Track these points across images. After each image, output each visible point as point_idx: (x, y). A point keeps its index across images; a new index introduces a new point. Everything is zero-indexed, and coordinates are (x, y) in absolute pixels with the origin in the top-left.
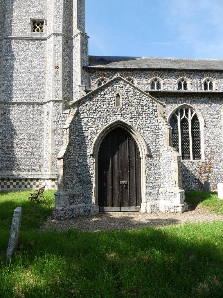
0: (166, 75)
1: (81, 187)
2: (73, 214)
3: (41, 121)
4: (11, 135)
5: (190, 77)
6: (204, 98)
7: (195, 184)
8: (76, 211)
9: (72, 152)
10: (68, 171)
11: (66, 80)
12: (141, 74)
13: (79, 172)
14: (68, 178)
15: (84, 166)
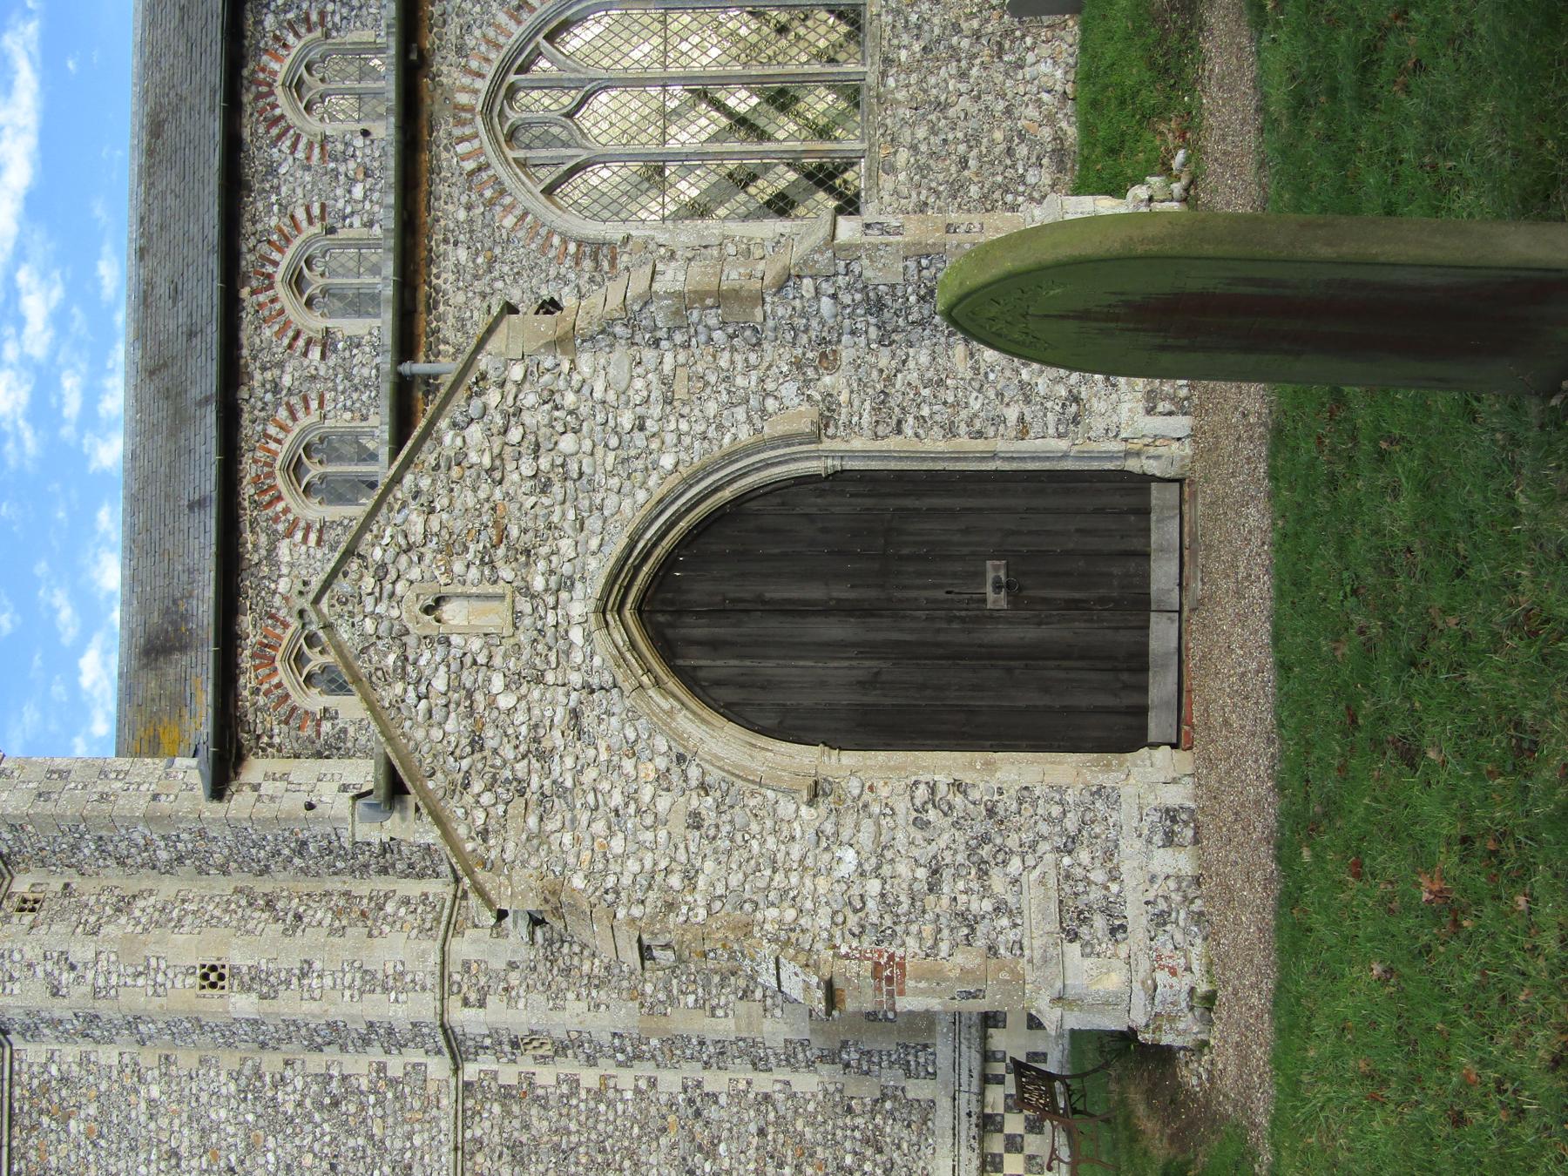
0: (269, 212)
1: (1015, 864)
2: (1182, 923)
3: (583, 1095)
5: (276, 38)
7: (1030, 57)
8: (1166, 898)
9: (790, 914)
10: (911, 942)
12: (259, 392)
13: (922, 873)
15: (884, 839)
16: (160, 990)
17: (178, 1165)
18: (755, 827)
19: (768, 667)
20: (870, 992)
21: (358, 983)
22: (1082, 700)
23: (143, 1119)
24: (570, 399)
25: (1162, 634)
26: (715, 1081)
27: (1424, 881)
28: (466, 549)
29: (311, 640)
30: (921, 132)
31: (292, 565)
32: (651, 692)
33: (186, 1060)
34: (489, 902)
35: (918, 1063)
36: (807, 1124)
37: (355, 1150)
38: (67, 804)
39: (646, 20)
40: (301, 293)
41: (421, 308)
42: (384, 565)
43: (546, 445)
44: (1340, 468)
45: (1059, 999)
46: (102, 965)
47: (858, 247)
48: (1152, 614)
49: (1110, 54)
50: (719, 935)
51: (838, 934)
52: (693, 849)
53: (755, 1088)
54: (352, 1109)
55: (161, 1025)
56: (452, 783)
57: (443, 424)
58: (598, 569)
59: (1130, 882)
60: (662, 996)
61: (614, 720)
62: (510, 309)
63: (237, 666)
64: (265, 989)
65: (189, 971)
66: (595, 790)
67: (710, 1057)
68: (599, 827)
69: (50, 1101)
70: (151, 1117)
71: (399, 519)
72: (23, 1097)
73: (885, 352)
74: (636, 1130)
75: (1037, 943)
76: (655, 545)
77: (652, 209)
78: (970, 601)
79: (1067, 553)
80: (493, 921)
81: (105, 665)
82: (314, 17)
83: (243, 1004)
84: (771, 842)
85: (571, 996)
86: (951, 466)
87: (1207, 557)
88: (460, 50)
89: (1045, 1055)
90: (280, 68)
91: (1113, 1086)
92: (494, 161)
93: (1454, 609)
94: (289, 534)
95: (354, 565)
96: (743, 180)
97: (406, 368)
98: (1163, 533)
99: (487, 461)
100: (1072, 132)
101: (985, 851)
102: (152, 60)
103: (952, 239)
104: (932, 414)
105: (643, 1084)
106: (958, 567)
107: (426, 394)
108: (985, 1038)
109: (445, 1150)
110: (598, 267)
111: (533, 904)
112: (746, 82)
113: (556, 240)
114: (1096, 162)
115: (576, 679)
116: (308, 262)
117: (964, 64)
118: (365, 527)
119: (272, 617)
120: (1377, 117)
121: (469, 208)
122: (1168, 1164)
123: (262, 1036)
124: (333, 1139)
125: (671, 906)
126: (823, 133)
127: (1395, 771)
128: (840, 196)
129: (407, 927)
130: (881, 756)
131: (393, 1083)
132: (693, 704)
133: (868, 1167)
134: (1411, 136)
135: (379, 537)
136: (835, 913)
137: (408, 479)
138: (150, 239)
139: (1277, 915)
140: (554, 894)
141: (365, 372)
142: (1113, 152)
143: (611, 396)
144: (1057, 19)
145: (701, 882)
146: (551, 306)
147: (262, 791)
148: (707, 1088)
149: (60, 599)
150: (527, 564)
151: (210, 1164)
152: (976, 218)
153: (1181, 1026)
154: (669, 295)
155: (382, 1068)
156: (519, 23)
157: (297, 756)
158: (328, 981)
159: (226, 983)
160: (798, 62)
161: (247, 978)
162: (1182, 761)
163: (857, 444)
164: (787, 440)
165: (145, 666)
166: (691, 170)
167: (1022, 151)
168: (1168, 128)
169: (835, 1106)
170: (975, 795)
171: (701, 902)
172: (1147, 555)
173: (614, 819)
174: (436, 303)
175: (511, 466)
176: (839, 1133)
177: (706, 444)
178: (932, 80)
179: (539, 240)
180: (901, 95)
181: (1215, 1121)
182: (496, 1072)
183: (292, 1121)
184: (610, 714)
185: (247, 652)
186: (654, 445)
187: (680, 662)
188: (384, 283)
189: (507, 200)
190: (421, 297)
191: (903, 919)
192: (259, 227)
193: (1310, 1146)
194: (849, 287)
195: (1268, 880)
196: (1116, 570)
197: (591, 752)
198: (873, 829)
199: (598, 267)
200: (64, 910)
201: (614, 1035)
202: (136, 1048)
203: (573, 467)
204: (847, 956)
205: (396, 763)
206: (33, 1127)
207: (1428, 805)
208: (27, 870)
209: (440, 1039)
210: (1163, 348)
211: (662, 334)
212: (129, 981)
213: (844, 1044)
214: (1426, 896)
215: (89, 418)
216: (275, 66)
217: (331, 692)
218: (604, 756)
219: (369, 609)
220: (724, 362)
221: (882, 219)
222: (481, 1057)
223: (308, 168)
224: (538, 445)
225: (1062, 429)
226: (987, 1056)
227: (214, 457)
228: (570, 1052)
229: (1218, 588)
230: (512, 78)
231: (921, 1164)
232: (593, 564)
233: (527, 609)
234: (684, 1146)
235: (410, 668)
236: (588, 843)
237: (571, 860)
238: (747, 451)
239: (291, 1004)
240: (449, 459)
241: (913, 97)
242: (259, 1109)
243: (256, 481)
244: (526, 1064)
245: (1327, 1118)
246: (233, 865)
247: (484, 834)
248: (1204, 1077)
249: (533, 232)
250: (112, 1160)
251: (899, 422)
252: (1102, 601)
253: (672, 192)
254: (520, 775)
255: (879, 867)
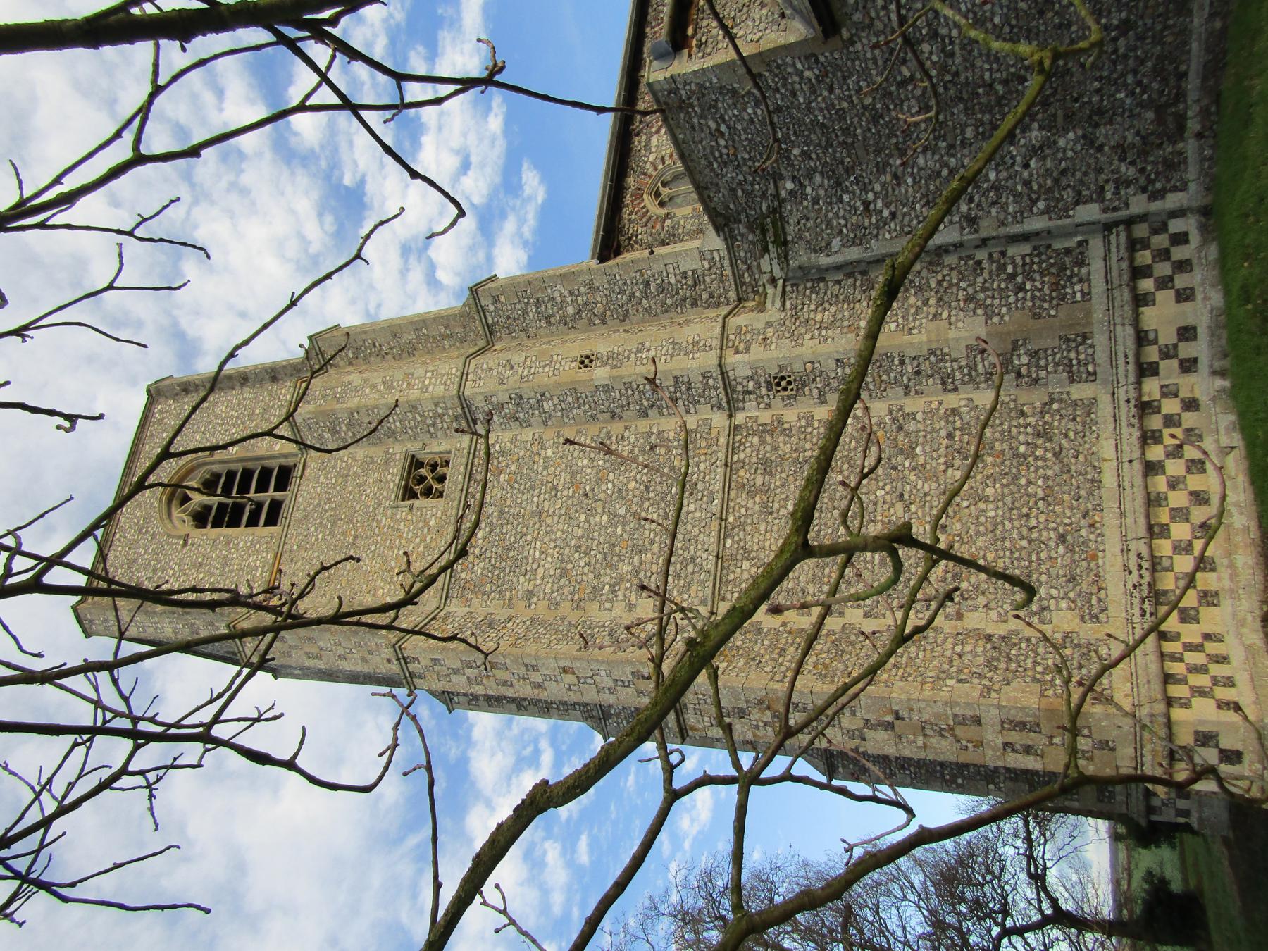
35: (1079, 361)
53: (945, 406)
67: (909, 380)
70: (545, 468)
74: (853, 443)
119: (644, 174)
148: (907, 410)
169: (1011, 410)
176: (1014, 430)
231: (1087, 446)
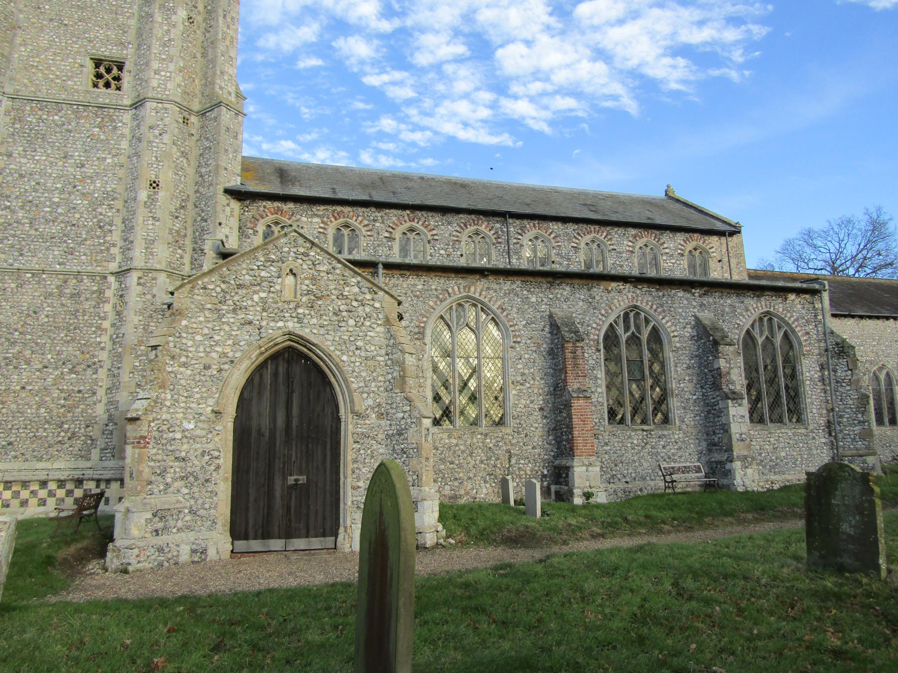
1: (186, 491)
4: (6, 358)
5: (493, 227)
6: (513, 282)
7: (488, 485)
9: (168, 403)
10: (155, 451)
11: (177, 217)
12: (374, 215)
13: (183, 454)
14: (152, 468)
16: (150, 166)
17: (78, 167)
18: (204, 390)
19: (267, 395)
20: (134, 435)
21: (150, 238)
22: (251, 515)
23: (98, 155)
24: (368, 324)
25: (276, 544)
26: (102, 373)
27: (163, 659)
28: (314, 285)
29: (283, 227)
30: (462, 447)
31: (311, 222)
32: (258, 351)
33: (121, 173)
34: (177, 289)
36: (83, 409)
37: (80, 234)
38: (224, 137)
39: (499, 352)
40: (408, 231)
41: (402, 272)
42: (308, 256)
43: (351, 314)
44: (333, 611)
45: (128, 510)
46: (161, 146)
47: (421, 426)
48: (283, 541)
49: (488, 514)
50: (160, 376)
51: (159, 422)
52: (196, 366)
54: (98, 234)
55: (136, 165)
56: (225, 277)
57: (359, 278)
58: (305, 332)
59: (177, 536)
60: (139, 353)
61: (248, 337)
62: (400, 303)
63: (275, 201)
64: (148, 204)
65: (157, 176)
66: (221, 329)
68: (206, 331)
69: (107, 122)
71: (325, 262)
72: (109, 112)
73: (384, 437)
75: (152, 500)
76: (314, 353)
77: (435, 353)
78: (291, 470)
79: (309, 506)
80: (170, 290)
81: (289, 150)
82: (499, 240)
83: (143, 195)
84: (198, 396)
85: (141, 318)
86: (342, 462)
87: (306, 560)
88: (488, 288)
89: (108, 504)
90: (482, 228)
91: (91, 534)
92: (452, 299)
93: (274, 661)
94: (323, 222)
95: (308, 245)
96: (446, 385)
97: (380, 266)
98: (316, 543)
99: (346, 293)
100: (462, 501)
101: (191, 479)
102: (486, 186)
103: (423, 460)
104: (361, 454)
105: (103, 345)
106: (304, 465)
107: (371, 272)
108: (116, 480)
109: (79, 268)
110: (416, 333)
111: (176, 305)
112: (479, 386)
113: (425, 319)
114: (452, 511)
115: (264, 323)
116: (418, 234)
117: (485, 462)
118: (322, 249)
119: (293, 214)
120: (460, 615)
121: (436, 290)
122: (54, 558)
123: (130, 201)
124: (85, 226)
125: (173, 358)
126: (462, 413)
127: (211, 642)
128: (440, 419)
129: (172, 257)
130: (231, 437)
131: (108, 249)
132: (254, 367)
133: (62, 434)
134: (452, 628)
135: (318, 254)
136: (168, 421)
137: (340, 266)
138: (427, 181)
139: (157, 598)
140: (180, 313)
141: (380, 251)
142: (455, 517)
143: (368, 338)
144: (501, 494)
145: (182, 369)
146: (401, 317)
147: (227, 207)
148: (100, 370)
149: (314, 136)
150: (308, 307)
151: (78, 179)
152: (431, 468)
153: (115, 560)
154: (404, 359)
155: (114, 245)
156: (498, 309)
157: (240, 220)
158: (151, 227)
159: (152, 189)
160: (486, 404)
161: (153, 197)
162: (226, 555)
163: (350, 427)
164: (352, 401)
165: (276, 169)
166: (449, 366)
167: (456, 484)
168: (463, 537)
169: (90, 421)
170: (214, 474)
171: (174, 369)
172: (307, 537)
173: (208, 336)
174: (403, 277)
175: (343, 302)
176: (78, 422)
177: (351, 372)
178: (480, 451)
179: (425, 313)
180: (475, 440)
181: (72, 577)
182: (110, 288)
183: (94, 210)
184: (250, 336)
185: (279, 205)
186: (350, 353)
187: (269, 362)
188: (411, 260)
189: (438, 303)
190: (405, 272)
191: (164, 448)
192: (430, 218)
193: (52, 619)
194: (407, 423)
195: (174, 593)
196: (302, 525)
197: (235, 329)
198: (202, 435)
199: (416, 333)
200: (183, 133)
201: (124, 334)
202: (127, 155)
203: (343, 324)
204: (149, 426)
205: (233, 257)
206: (96, 115)
207: (196, 657)
208: (199, 121)
209: (125, 268)
210: (370, 544)
211: (390, 357)
212: (154, 155)
213: (116, 424)
214: (156, 660)
215: (379, 151)
216: (484, 226)
217: (264, 234)
218: (234, 333)
219: (292, 249)
220: (380, 378)
221: (431, 435)
222: (117, 283)
223: (450, 236)
224: (351, 312)
225: (355, 502)
226: (108, 481)
227: (351, 198)
228: (117, 317)
229: (294, 565)
230: (480, 306)
231: (63, 456)
232: (307, 330)
233: (291, 306)
234: (75, 361)
235: (269, 263)
236: (200, 327)
237: (193, 320)
238: (348, 387)
239: (141, 214)
240: (346, 280)
241: (474, 444)
242: (100, 199)
243: (342, 212)
244: (113, 300)
245: (65, 625)
246: (198, 195)
247: (205, 288)
248: (92, 571)
249: (427, 311)
250: (81, 143)
251: (358, 442)
252: (290, 520)
253: (441, 360)
254: (227, 302)
255: (186, 437)
